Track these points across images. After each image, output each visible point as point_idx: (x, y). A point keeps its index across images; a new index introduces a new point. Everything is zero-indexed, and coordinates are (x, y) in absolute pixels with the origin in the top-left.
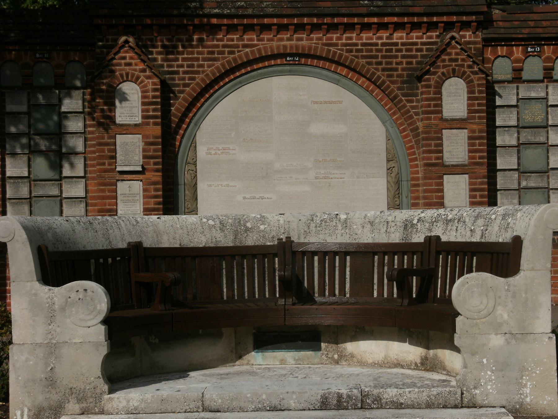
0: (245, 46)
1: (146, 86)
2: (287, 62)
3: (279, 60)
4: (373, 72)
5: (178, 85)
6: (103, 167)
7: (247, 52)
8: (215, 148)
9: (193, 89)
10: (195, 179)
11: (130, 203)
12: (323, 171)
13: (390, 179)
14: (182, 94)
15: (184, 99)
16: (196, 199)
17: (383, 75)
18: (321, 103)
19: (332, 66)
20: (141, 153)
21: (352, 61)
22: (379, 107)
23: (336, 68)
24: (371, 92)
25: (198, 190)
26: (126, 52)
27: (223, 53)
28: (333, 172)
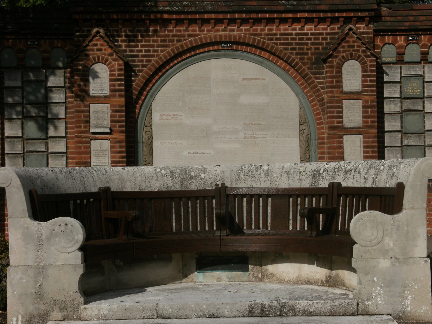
0: (190, 36)
1: (113, 66)
2: (222, 48)
3: (216, 47)
4: (289, 55)
5: (138, 66)
6: (80, 129)
7: (191, 40)
8: (166, 115)
9: (150, 69)
10: (151, 139)
11: (101, 157)
12: (250, 133)
13: (302, 138)
14: (141, 72)
15: (143, 77)
16: (152, 154)
17: (297, 58)
18: (249, 80)
19: (257, 51)
20: (109, 118)
21: (272, 47)
22: (293, 83)
23: (260, 53)
24: (287, 71)
25: (153, 147)
26: (98, 40)
27: (172, 41)
28: (258, 133)
